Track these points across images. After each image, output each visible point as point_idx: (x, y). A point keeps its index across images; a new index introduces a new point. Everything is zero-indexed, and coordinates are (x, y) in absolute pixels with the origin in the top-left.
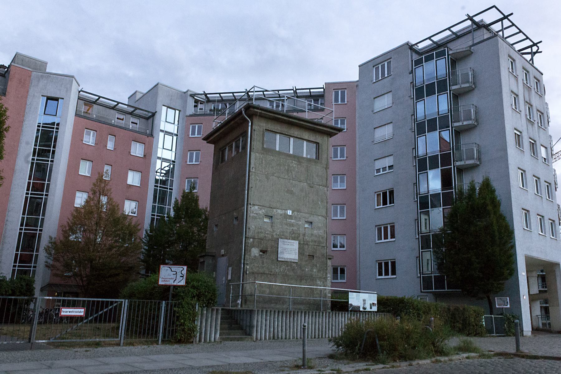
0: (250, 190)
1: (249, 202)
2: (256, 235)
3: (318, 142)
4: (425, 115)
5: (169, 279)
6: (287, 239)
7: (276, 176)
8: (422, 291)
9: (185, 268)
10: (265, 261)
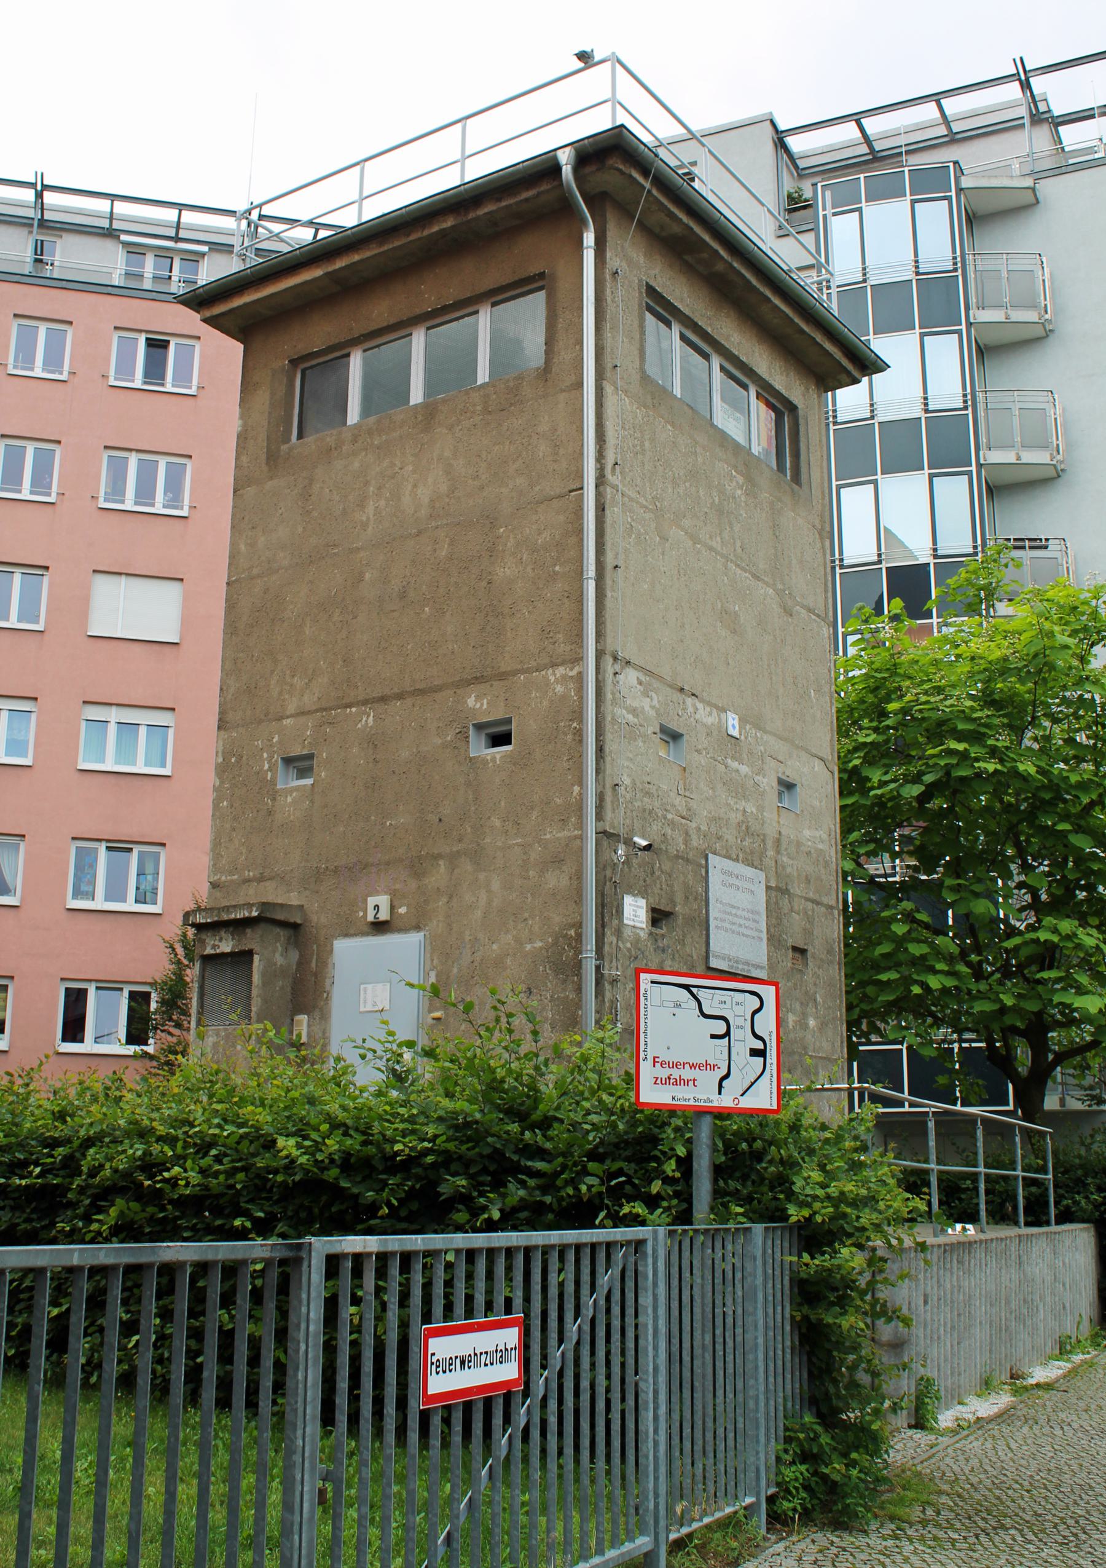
0: (608, 582)
1: (610, 644)
5: (692, 1066)
6: (729, 857)
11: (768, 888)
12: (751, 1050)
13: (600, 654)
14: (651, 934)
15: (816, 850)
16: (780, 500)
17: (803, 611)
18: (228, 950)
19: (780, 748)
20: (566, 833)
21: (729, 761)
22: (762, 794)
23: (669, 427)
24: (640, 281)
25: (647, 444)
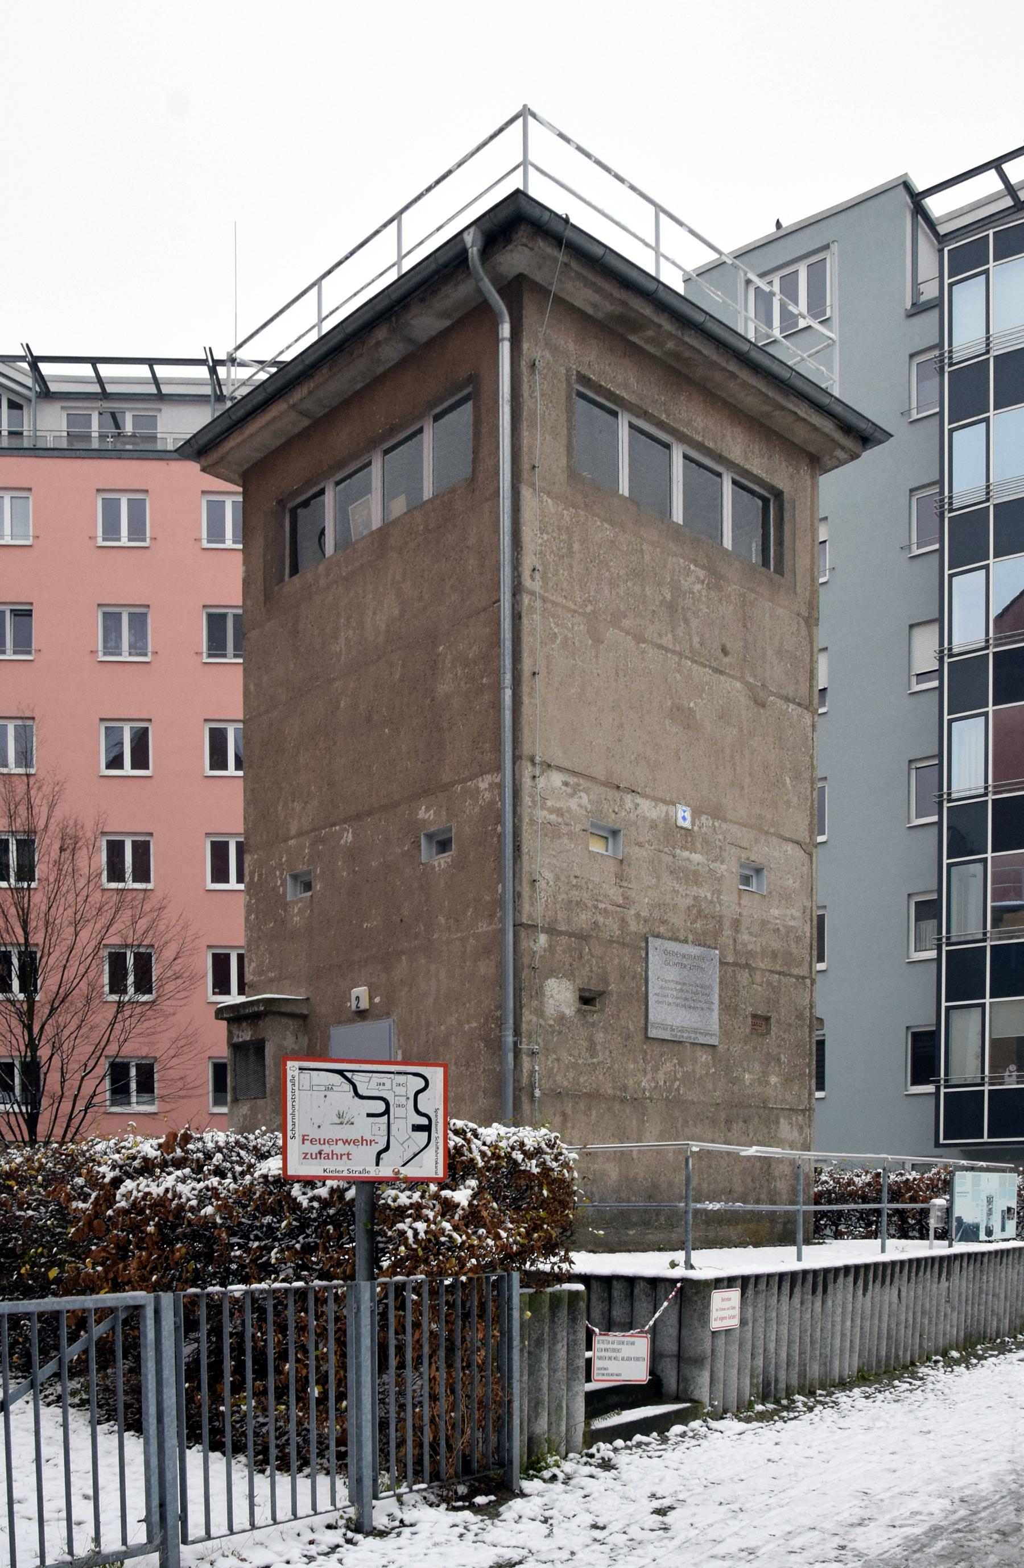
0: (525, 689)
1: (526, 749)
2: (560, 915)
3: (780, 486)
4: (988, 487)
5: (346, 1142)
7: (628, 633)
8: (942, 1141)
9: (436, 1075)
10: (600, 1037)
11: (722, 963)
12: (413, 1126)
13: (516, 758)
14: (579, 1011)
15: (785, 926)
16: (753, 591)
17: (778, 701)
18: (248, 1038)
19: (746, 836)
20: (494, 926)
21: (678, 851)
22: (720, 879)
23: (606, 525)
24: (568, 370)
25: (576, 546)
